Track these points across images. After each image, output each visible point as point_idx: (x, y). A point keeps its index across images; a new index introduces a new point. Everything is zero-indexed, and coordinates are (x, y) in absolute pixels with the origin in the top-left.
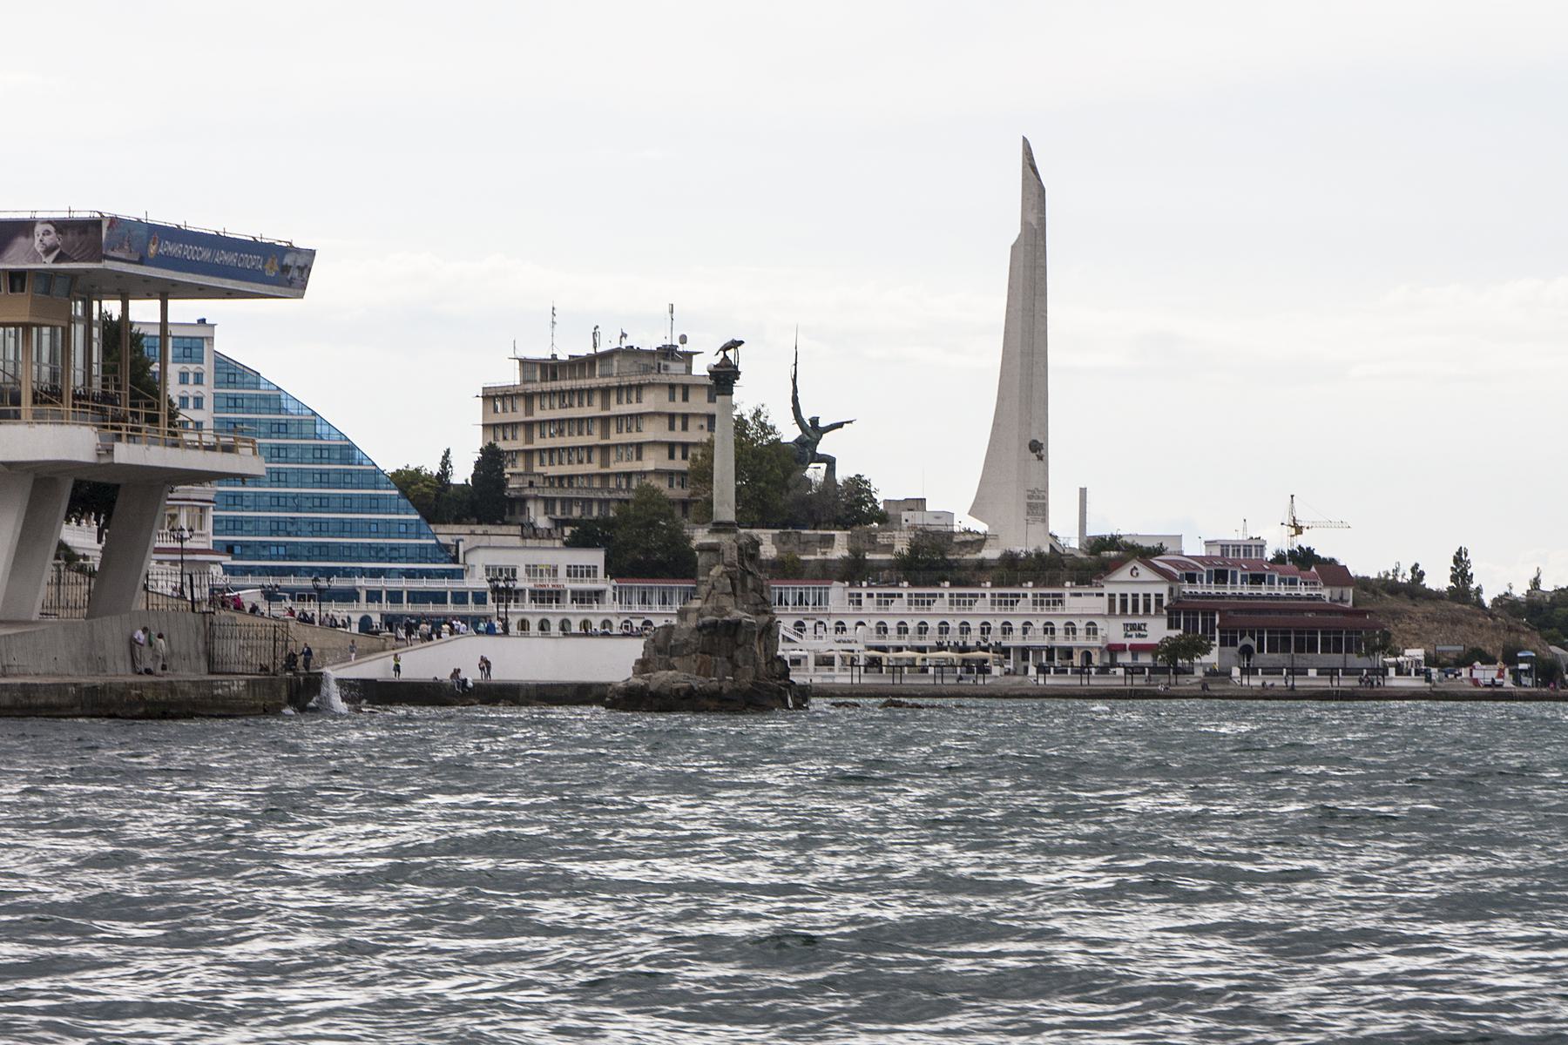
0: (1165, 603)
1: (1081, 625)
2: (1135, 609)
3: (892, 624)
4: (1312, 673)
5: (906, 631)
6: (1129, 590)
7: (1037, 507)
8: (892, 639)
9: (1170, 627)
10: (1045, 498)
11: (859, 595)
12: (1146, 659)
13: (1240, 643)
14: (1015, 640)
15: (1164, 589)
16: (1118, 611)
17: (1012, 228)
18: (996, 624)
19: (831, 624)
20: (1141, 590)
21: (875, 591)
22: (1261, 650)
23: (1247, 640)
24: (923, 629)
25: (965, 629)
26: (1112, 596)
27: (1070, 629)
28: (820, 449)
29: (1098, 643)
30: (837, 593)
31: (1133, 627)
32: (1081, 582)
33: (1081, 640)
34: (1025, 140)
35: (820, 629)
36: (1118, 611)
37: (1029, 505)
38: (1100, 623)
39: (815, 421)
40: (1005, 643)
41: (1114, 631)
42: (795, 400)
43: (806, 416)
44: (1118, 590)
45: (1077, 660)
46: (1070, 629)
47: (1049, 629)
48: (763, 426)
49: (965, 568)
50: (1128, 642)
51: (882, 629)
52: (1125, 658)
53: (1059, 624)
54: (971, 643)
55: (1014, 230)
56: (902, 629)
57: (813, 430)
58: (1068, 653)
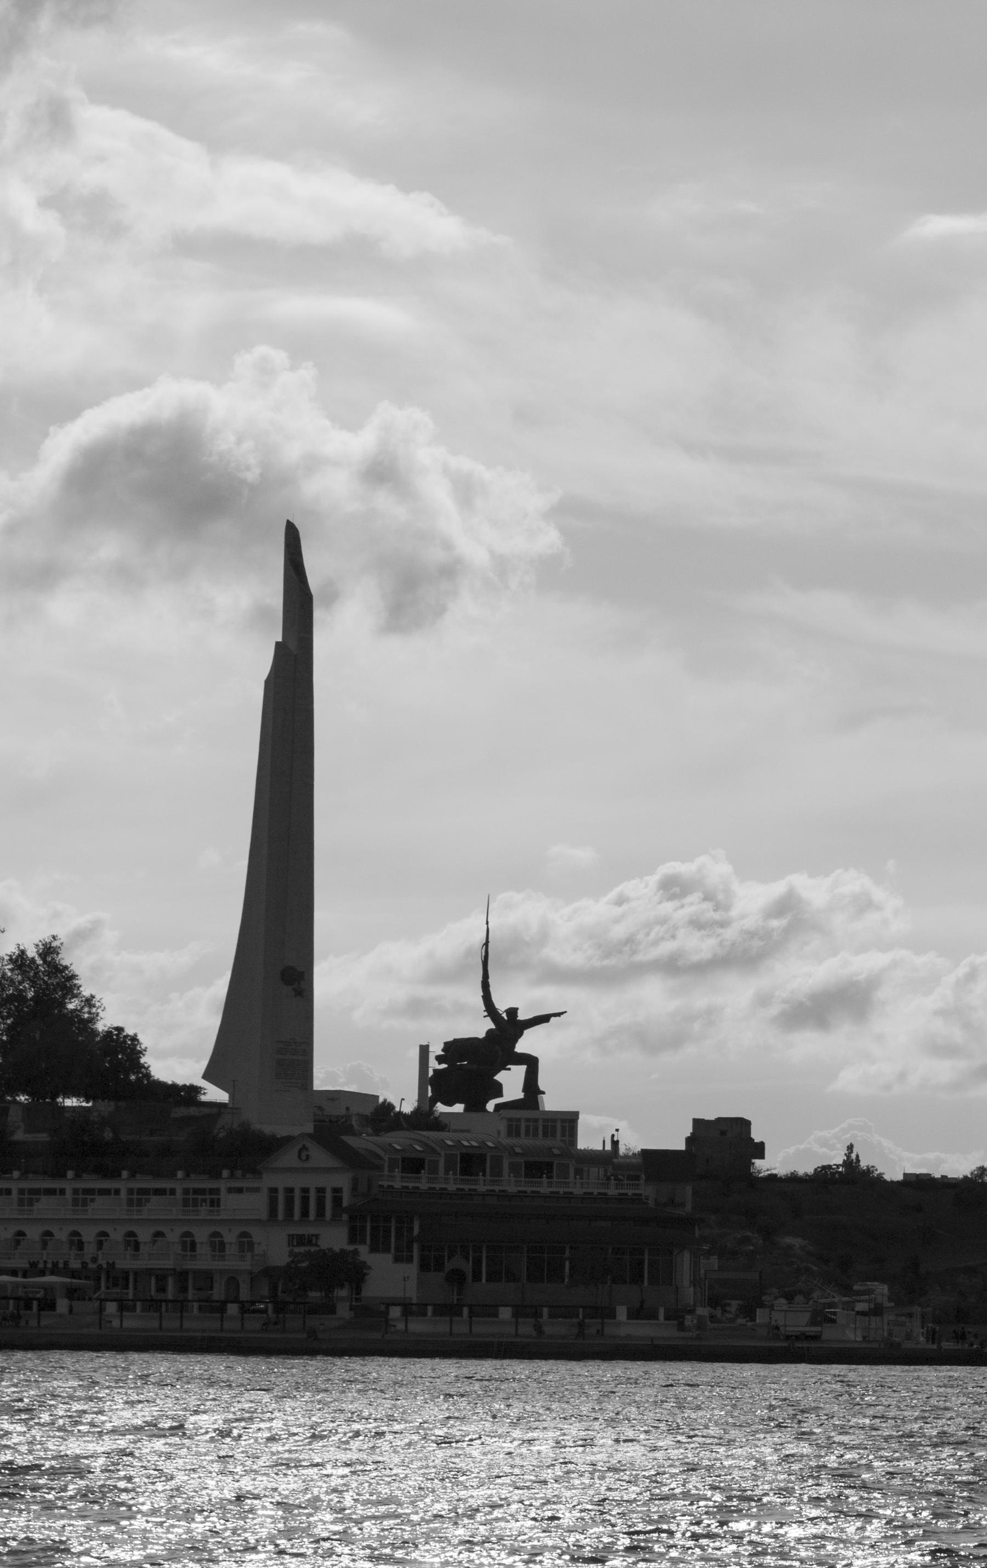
0: (345, 1203)
2: (305, 1213)
4: (505, 1313)
6: (297, 1182)
11: (217, 1191)
13: (448, 1266)
15: (343, 1181)
20: (312, 1182)
22: (477, 1277)
23: (457, 1262)
26: (274, 1191)
28: (522, 1046)
33: (233, 1262)
38: (257, 1234)
39: (512, 1012)
43: (502, 1005)
44: (281, 1181)
45: (218, 1292)
47: (189, 1245)
58: (207, 1278)
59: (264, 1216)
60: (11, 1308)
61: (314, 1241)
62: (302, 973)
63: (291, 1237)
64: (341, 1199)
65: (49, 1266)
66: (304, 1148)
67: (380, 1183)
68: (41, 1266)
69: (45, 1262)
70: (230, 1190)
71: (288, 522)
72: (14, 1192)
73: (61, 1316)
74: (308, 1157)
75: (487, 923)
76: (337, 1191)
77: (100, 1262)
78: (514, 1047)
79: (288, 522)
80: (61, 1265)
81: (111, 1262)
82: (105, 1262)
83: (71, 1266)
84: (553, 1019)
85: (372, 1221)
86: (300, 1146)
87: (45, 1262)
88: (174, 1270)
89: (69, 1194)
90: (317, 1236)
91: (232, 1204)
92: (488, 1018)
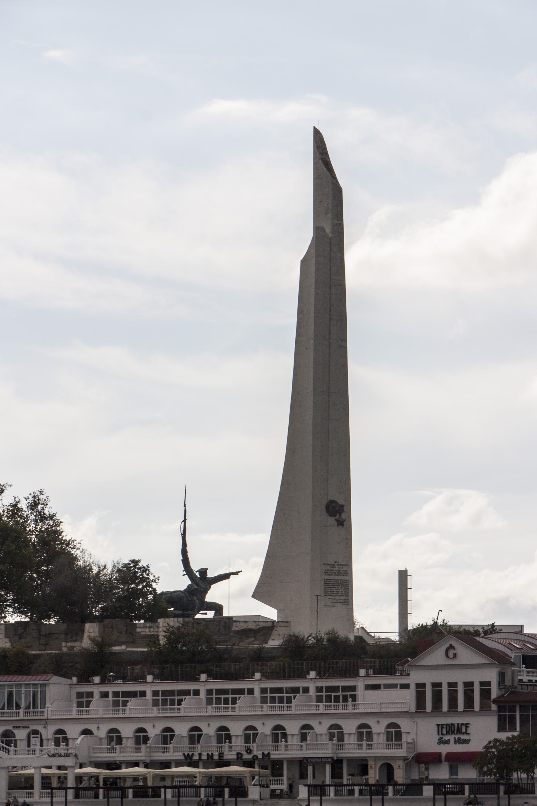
0: (494, 695)
1: (378, 728)
3: (127, 731)
5: (146, 739)
6: (444, 678)
7: (337, 584)
8: (126, 752)
9: (501, 728)
10: (348, 573)
11: (353, 688)
12: (468, 774)
14: (291, 751)
15: (491, 675)
16: (429, 707)
17: (301, 238)
18: (265, 729)
19: (48, 733)
20: (460, 677)
21: (110, 689)
24: (168, 735)
25: (223, 735)
26: (421, 686)
27: (365, 733)
28: (211, 597)
29: (402, 752)
30: (58, 692)
31: (451, 729)
32: (380, 671)
33: (380, 749)
34: (317, 132)
35: (35, 741)
36: (429, 707)
37: (327, 583)
38: (405, 725)
39: (203, 572)
40: (275, 755)
41: (423, 735)
42: (184, 552)
43: (195, 567)
44: (428, 678)
45: (373, 776)
46: (365, 733)
47: (336, 734)
48: (43, 518)
49: (238, 660)
50: (444, 749)
51: (115, 738)
52: (441, 773)
53: (350, 727)
54: (230, 755)
55: (305, 237)
56: (141, 738)
57: (202, 581)
58: (362, 766)
59: (413, 709)
60: (202, 796)
61: (464, 730)
62: (343, 506)
63: (440, 727)
64: (489, 691)
65: (204, 757)
66: (451, 647)
67: (519, 677)
68: (196, 757)
69: (200, 754)
70: (370, 687)
71: (314, 127)
72: (111, 695)
73: (254, 801)
74: (455, 655)
75: (185, 506)
76: (485, 685)
77: (255, 752)
78: (205, 598)
79: (314, 127)
80: (216, 757)
81: (266, 752)
82: (261, 752)
83: (225, 757)
84: (232, 576)
85: (520, 711)
86: (448, 645)
87: (200, 754)
88: (332, 758)
89: (203, 695)
90: (467, 725)
91: (369, 700)
92: (187, 576)
